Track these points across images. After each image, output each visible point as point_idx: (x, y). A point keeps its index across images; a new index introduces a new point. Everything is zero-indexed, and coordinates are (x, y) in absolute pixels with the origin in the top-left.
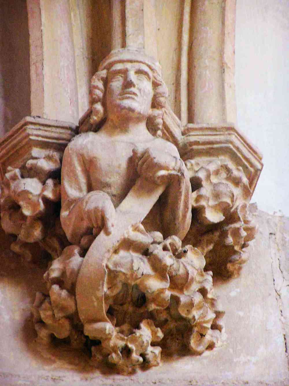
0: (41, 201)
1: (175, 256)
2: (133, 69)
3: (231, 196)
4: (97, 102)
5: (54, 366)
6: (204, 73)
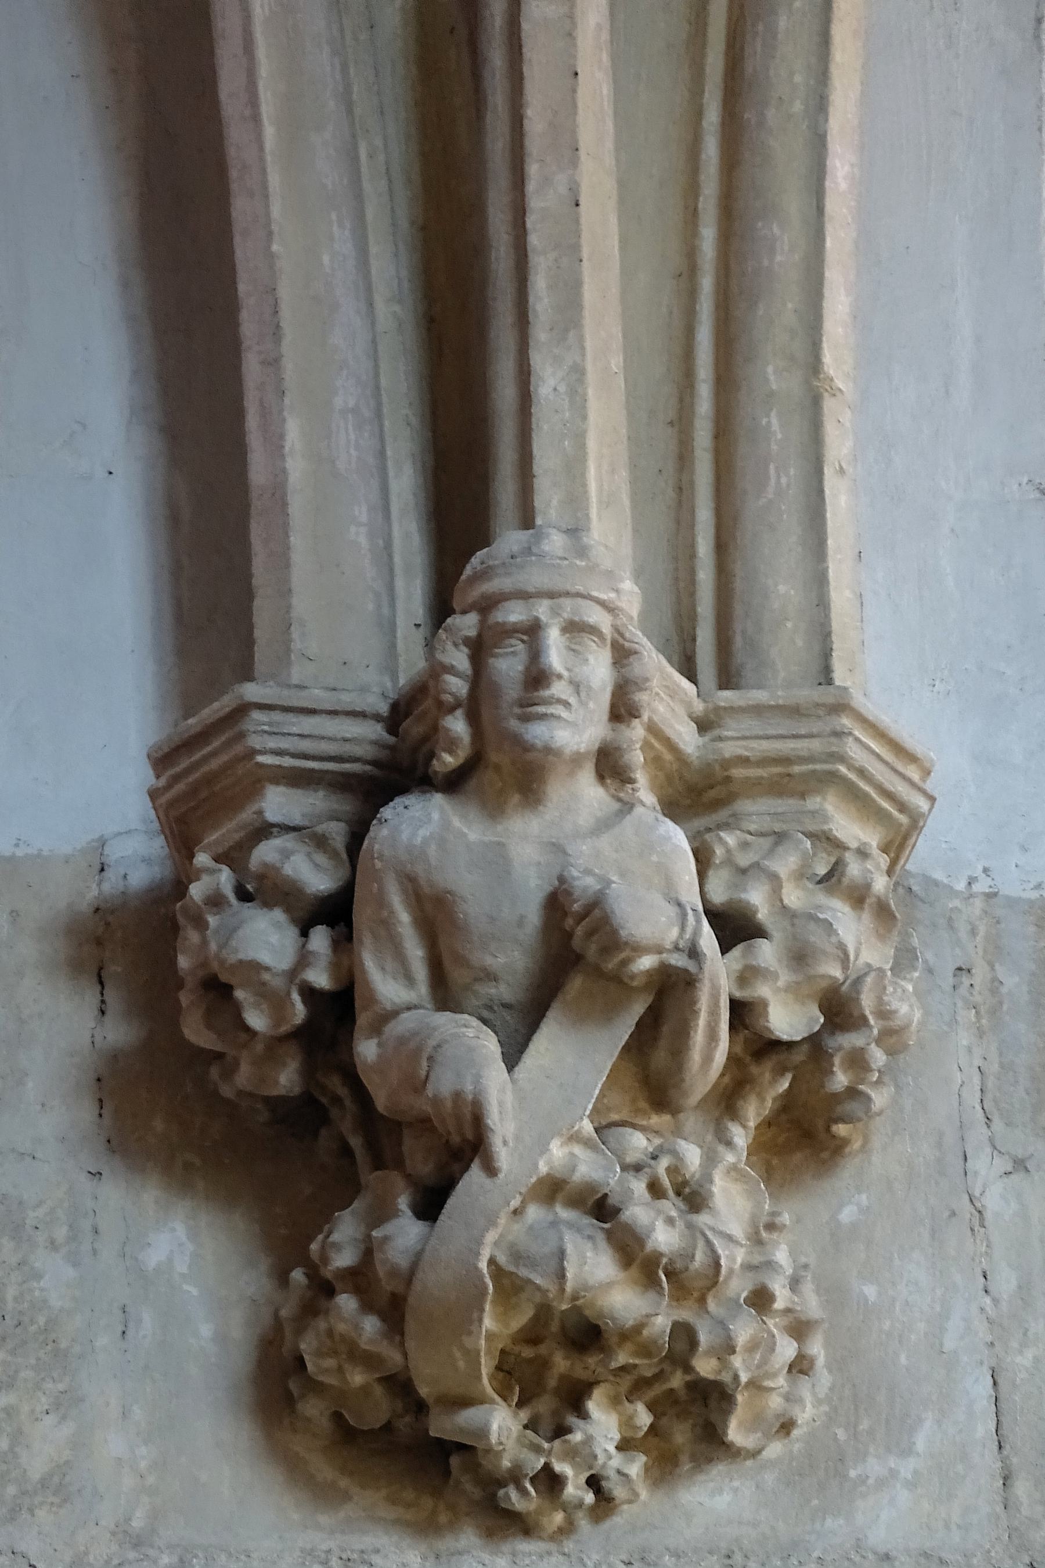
0: (296, 997)
1: (681, 1198)
2: (556, 621)
3: (842, 956)
4: (452, 710)
5: (347, 1510)
6: (764, 421)
